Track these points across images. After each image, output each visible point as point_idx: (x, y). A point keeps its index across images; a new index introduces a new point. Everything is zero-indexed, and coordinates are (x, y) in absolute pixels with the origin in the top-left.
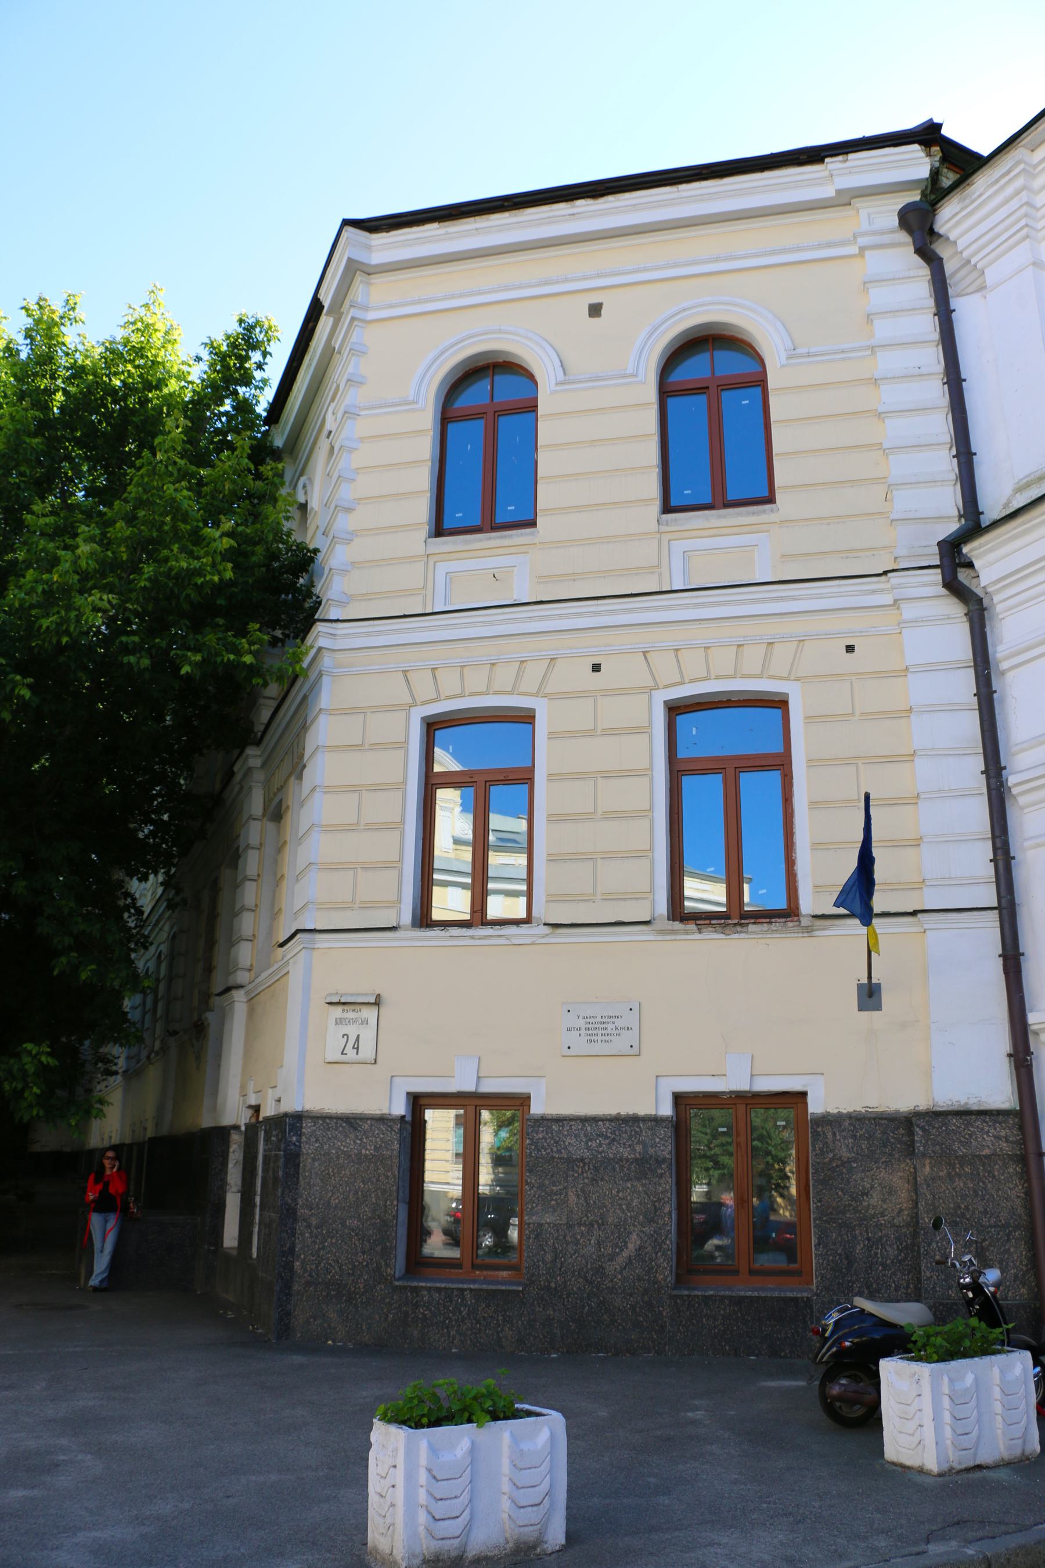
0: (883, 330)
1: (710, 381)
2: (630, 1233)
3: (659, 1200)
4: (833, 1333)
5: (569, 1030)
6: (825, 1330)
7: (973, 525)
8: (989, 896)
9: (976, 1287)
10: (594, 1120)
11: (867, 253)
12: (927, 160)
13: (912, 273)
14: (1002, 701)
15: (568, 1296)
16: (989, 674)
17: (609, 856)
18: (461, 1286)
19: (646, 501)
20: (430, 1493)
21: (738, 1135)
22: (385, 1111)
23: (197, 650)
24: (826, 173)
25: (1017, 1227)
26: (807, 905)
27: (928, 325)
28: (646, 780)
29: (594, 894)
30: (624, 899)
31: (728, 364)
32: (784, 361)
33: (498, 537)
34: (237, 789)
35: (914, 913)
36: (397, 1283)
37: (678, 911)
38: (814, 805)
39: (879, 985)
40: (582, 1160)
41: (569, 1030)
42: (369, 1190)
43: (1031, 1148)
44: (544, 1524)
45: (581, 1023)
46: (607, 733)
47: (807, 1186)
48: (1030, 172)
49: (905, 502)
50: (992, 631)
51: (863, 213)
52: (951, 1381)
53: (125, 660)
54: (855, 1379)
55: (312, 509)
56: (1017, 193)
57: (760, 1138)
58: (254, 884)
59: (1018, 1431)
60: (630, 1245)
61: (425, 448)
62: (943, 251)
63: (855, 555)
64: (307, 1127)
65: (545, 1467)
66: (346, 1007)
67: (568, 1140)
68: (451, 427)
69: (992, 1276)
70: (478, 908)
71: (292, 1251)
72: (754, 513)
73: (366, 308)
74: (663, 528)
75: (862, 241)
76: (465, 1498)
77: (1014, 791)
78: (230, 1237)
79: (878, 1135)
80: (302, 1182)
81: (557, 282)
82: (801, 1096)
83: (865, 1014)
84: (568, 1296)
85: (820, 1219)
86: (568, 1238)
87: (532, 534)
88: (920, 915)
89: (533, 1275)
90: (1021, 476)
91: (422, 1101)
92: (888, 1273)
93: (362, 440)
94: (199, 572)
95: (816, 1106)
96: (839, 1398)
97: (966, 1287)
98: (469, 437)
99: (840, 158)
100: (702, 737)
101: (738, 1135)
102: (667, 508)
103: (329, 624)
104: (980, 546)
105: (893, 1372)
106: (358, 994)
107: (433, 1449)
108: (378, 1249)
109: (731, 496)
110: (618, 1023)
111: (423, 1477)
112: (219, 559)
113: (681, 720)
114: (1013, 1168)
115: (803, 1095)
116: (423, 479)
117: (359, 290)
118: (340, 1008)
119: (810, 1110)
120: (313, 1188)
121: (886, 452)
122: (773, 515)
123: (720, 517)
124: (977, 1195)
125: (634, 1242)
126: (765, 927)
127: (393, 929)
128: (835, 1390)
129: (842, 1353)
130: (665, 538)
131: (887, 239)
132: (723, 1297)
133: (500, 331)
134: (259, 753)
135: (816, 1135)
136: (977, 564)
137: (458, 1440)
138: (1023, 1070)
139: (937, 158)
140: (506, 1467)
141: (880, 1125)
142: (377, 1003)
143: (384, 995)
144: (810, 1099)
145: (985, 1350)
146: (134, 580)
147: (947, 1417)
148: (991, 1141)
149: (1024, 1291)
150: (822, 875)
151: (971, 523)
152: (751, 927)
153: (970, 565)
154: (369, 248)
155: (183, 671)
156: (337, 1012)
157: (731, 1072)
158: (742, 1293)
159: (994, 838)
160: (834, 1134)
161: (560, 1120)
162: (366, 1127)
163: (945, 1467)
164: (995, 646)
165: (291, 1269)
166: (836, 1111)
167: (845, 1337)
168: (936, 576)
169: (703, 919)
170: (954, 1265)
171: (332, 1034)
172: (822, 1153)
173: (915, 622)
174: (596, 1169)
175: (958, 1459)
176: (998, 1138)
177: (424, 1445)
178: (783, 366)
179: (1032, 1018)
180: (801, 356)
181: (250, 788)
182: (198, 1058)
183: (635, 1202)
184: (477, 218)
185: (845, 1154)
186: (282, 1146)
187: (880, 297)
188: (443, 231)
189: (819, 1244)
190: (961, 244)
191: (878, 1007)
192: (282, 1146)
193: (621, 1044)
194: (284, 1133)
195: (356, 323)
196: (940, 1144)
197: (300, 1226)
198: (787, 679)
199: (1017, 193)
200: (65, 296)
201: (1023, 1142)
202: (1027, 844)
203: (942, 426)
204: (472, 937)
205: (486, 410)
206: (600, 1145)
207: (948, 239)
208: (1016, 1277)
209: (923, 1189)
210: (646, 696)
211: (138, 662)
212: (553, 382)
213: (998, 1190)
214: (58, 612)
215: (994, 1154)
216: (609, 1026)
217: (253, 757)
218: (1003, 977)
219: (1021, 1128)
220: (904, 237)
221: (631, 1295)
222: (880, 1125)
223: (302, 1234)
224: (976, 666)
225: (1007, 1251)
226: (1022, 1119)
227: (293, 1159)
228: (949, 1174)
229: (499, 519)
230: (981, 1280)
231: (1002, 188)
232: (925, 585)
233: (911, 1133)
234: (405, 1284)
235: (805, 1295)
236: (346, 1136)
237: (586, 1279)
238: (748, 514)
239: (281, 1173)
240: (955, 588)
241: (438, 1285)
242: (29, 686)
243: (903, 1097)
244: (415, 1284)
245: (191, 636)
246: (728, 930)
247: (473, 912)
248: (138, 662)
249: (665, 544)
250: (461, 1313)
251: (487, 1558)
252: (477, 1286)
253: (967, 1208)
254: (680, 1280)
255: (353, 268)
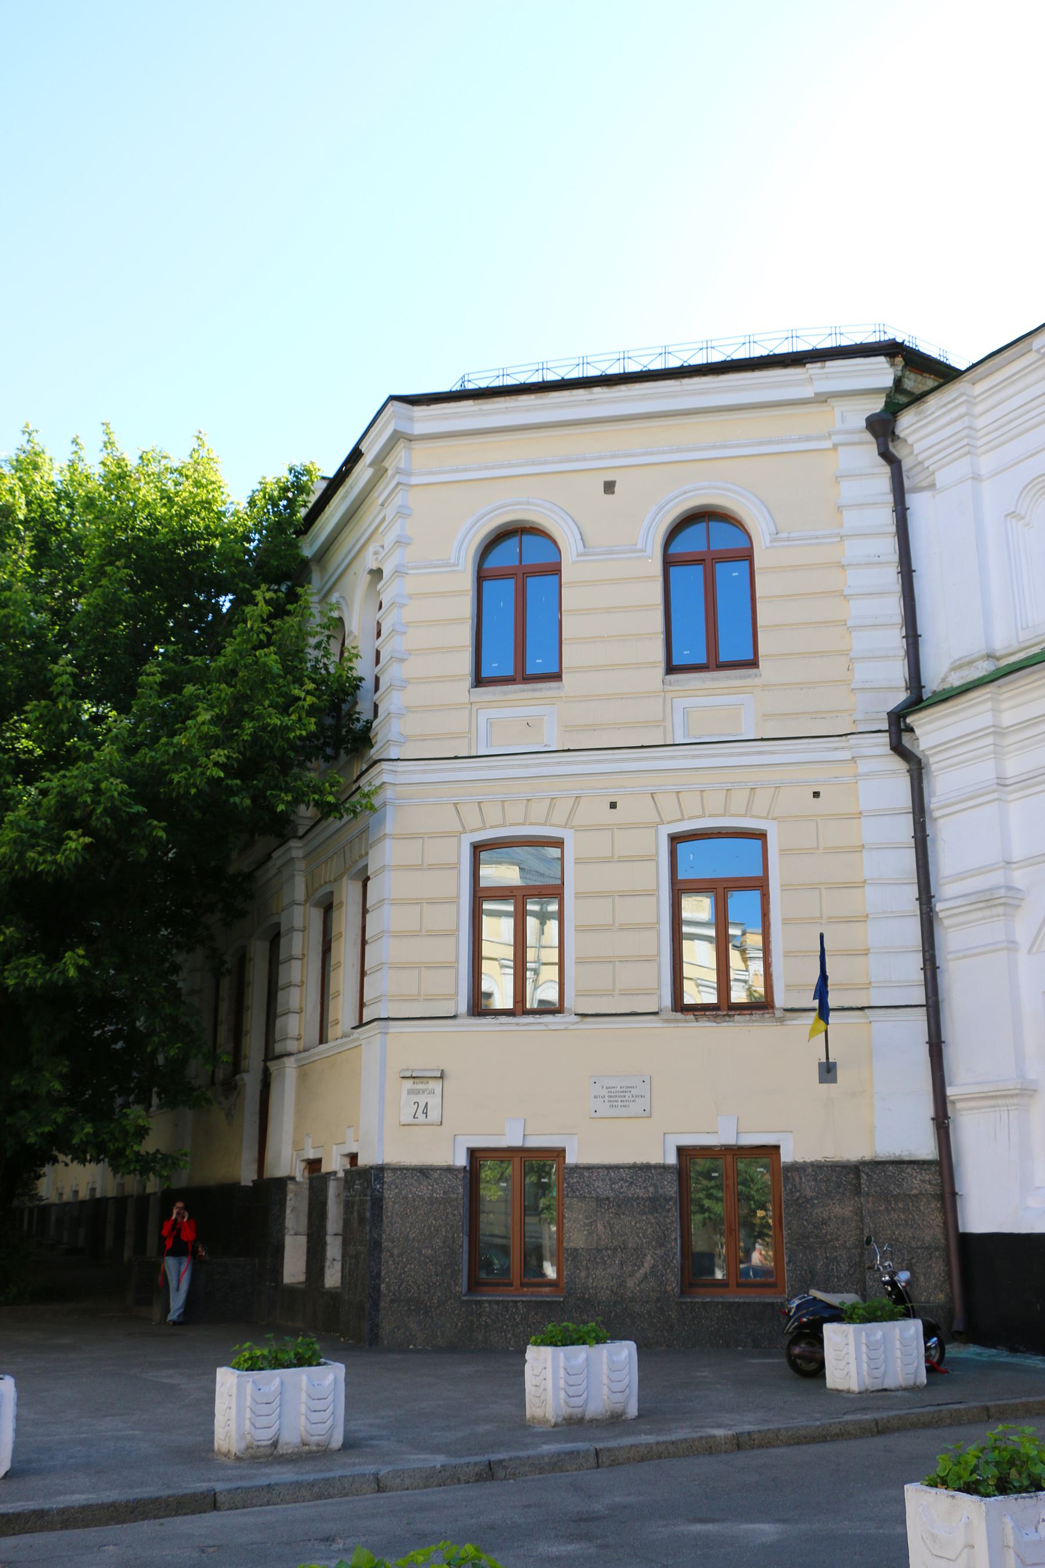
0: (851, 520)
1: (705, 550)
2: (645, 1255)
3: (668, 1229)
4: (795, 1313)
5: (595, 1097)
6: (790, 1311)
7: (918, 699)
8: (919, 996)
9: (893, 1283)
10: (617, 1168)
11: (840, 448)
12: (891, 370)
13: (876, 470)
14: (934, 841)
15: (599, 1304)
16: (924, 821)
17: (624, 960)
18: (514, 1299)
19: (653, 665)
20: (566, 1382)
21: (727, 1178)
22: (450, 1163)
23: (287, 790)
24: (806, 376)
25: (937, 1249)
26: (780, 1000)
27: (886, 517)
28: (654, 899)
29: (614, 990)
30: (638, 994)
31: (721, 537)
32: (768, 544)
33: (531, 690)
34: (273, 871)
35: (862, 1009)
36: (464, 1298)
37: (679, 1005)
38: (786, 921)
39: (835, 1064)
40: (608, 1199)
41: (595, 1097)
42: (440, 1226)
43: (947, 1189)
44: (626, 1404)
45: (605, 1092)
46: (623, 860)
47: (780, 1218)
48: (971, 402)
49: (863, 673)
50: (928, 782)
51: (838, 411)
52: (867, 1335)
53: (232, 800)
54: (809, 1344)
55: (351, 633)
56: (961, 417)
57: (744, 1183)
58: (300, 962)
59: (911, 1369)
60: (646, 1265)
61: (466, 607)
62: (898, 451)
63: (823, 716)
64: (388, 1176)
65: (626, 1371)
66: (416, 1080)
67: (597, 1184)
68: (486, 585)
69: (903, 1276)
70: (519, 999)
71: (379, 1274)
72: (741, 678)
73: (410, 474)
74: (668, 688)
75: (836, 439)
76: (584, 1385)
77: (941, 915)
78: (294, 1268)
79: (834, 1179)
80: (385, 1221)
81: (577, 460)
82: (774, 1150)
83: (825, 1086)
84: (599, 1304)
85: (790, 1243)
86: (598, 1260)
87: (558, 688)
88: (866, 1011)
89: (571, 1289)
90: (956, 658)
91: (478, 1155)
92: (842, 1284)
93: (410, 596)
94: (288, 729)
95: (787, 1156)
96: (799, 1356)
97: (886, 1283)
98: (501, 592)
99: (819, 365)
100: (698, 863)
101: (727, 1178)
102: (671, 669)
103: (391, 763)
104: (920, 719)
105: (830, 1330)
106: (426, 1070)
107: (567, 1358)
108: (449, 1272)
109: (723, 658)
110: (634, 1092)
111: (562, 1373)
112: (304, 715)
113: (681, 847)
114: (935, 1204)
115: (777, 1148)
116: (465, 635)
117: (400, 457)
118: (411, 1081)
119: (783, 1160)
120: (397, 1225)
121: (850, 630)
122: (756, 679)
123: (713, 679)
124: (907, 1224)
125: (649, 1261)
126: (748, 1017)
127: (454, 1017)
128: (797, 1350)
129: (802, 1326)
130: (669, 695)
131: (855, 438)
132: (718, 1303)
133: (528, 503)
134: (300, 845)
135: (787, 1178)
136: (918, 731)
137: (580, 1353)
138: (942, 1131)
139: (900, 368)
140: (605, 1367)
141: (835, 1171)
142: (441, 1077)
143: (446, 1070)
144: (783, 1151)
145: (892, 1317)
146: (237, 734)
147: (865, 1358)
148: (918, 1183)
149: (941, 1296)
150: (794, 987)
151: (915, 696)
152: (737, 1018)
153: (911, 730)
154: (411, 419)
155: (279, 809)
156: (409, 1084)
157: (723, 1134)
158: (732, 1300)
159: (924, 951)
160: (800, 1178)
161: (589, 1168)
162: (437, 1175)
163: (863, 1388)
164: (930, 796)
165: (379, 1290)
166: (801, 1160)
167: (803, 1316)
168: (885, 738)
169: (699, 1010)
170: (879, 1269)
171: (404, 1102)
172: (792, 1192)
173: (868, 775)
174: (619, 1206)
175: (870, 1384)
176: (923, 1181)
177: (562, 1355)
178: (767, 548)
179: (950, 1091)
180: (782, 540)
181: (293, 876)
182: (229, 1115)
183: (649, 1230)
184: (507, 398)
185: (809, 1193)
186: (369, 1192)
187: (849, 490)
188: (477, 408)
189: (789, 1262)
190: (917, 448)
191: (834, 1080)
192: (369, 1192)
193: (636, 1108)
194: (366, 1181)
195: (400, 487)
196: (880, 1186)
197: (385, 1255)
198: (766, 818)
199: (961, 417)
200: (140, 453)
201: (942, 1185)
202: (949, 957)
203: (894, 607)
204: (517, 1024)
205: (516, 565)
206: (622, 1187)
207: (906, 441)
208: (936, 1285)
209: (868, 1220)
210: (653, 830)
211: (241, 802)
212: (575, 554)
213: (924, 1220)
214: (185, 769)
215: (921, 1193)
216: (627, 1095)
217: (296, 849)
218: (929, 1059)
219: (941, 1174)
220: (868, 437)
221: (647, 1302)
222: (835, 1171)
223: (387, 1262)
224: (914, 812)
225: (930, 1266)
226: (941, 1168)
227: (378, 1202)
228: (887, 1208)
229: (530, 670)
230: (896, 1278)
231: (949, 411)
232: (877, 745)
233: (858, 1178)
234: (471, 1298)
235: (779, 1300)
236: (420, 1184)
237: (612, 1291)
238: (736, 678)
239: (368, 1214)
240: (899, 749)
241: (497, 1298)
242: (164, 829)
243: (853, 1152)
244: (479, 1298)
245: (282, 778)
246: (718, 1019)
247: (515, 1002)
248: (241, 802)
249: (668, 701)
250: (515, 1319)
251: (597, 1420)
252: (528, 1299)
253: (900, 1235)
254: (683, 1293)
255: (397, 437)
